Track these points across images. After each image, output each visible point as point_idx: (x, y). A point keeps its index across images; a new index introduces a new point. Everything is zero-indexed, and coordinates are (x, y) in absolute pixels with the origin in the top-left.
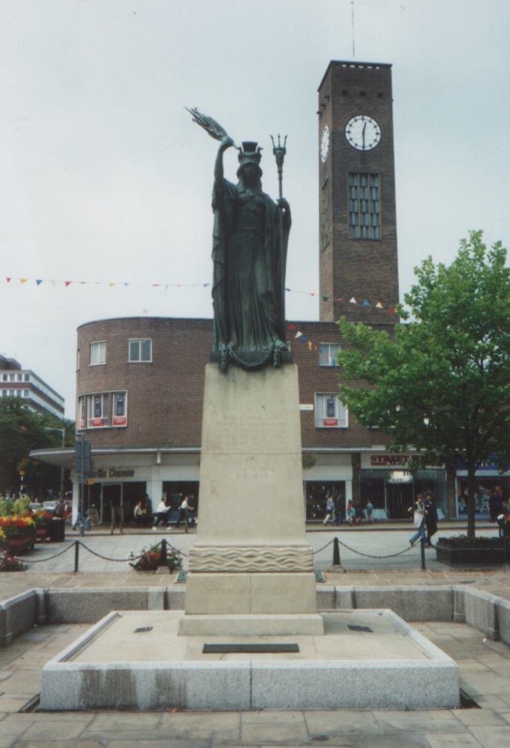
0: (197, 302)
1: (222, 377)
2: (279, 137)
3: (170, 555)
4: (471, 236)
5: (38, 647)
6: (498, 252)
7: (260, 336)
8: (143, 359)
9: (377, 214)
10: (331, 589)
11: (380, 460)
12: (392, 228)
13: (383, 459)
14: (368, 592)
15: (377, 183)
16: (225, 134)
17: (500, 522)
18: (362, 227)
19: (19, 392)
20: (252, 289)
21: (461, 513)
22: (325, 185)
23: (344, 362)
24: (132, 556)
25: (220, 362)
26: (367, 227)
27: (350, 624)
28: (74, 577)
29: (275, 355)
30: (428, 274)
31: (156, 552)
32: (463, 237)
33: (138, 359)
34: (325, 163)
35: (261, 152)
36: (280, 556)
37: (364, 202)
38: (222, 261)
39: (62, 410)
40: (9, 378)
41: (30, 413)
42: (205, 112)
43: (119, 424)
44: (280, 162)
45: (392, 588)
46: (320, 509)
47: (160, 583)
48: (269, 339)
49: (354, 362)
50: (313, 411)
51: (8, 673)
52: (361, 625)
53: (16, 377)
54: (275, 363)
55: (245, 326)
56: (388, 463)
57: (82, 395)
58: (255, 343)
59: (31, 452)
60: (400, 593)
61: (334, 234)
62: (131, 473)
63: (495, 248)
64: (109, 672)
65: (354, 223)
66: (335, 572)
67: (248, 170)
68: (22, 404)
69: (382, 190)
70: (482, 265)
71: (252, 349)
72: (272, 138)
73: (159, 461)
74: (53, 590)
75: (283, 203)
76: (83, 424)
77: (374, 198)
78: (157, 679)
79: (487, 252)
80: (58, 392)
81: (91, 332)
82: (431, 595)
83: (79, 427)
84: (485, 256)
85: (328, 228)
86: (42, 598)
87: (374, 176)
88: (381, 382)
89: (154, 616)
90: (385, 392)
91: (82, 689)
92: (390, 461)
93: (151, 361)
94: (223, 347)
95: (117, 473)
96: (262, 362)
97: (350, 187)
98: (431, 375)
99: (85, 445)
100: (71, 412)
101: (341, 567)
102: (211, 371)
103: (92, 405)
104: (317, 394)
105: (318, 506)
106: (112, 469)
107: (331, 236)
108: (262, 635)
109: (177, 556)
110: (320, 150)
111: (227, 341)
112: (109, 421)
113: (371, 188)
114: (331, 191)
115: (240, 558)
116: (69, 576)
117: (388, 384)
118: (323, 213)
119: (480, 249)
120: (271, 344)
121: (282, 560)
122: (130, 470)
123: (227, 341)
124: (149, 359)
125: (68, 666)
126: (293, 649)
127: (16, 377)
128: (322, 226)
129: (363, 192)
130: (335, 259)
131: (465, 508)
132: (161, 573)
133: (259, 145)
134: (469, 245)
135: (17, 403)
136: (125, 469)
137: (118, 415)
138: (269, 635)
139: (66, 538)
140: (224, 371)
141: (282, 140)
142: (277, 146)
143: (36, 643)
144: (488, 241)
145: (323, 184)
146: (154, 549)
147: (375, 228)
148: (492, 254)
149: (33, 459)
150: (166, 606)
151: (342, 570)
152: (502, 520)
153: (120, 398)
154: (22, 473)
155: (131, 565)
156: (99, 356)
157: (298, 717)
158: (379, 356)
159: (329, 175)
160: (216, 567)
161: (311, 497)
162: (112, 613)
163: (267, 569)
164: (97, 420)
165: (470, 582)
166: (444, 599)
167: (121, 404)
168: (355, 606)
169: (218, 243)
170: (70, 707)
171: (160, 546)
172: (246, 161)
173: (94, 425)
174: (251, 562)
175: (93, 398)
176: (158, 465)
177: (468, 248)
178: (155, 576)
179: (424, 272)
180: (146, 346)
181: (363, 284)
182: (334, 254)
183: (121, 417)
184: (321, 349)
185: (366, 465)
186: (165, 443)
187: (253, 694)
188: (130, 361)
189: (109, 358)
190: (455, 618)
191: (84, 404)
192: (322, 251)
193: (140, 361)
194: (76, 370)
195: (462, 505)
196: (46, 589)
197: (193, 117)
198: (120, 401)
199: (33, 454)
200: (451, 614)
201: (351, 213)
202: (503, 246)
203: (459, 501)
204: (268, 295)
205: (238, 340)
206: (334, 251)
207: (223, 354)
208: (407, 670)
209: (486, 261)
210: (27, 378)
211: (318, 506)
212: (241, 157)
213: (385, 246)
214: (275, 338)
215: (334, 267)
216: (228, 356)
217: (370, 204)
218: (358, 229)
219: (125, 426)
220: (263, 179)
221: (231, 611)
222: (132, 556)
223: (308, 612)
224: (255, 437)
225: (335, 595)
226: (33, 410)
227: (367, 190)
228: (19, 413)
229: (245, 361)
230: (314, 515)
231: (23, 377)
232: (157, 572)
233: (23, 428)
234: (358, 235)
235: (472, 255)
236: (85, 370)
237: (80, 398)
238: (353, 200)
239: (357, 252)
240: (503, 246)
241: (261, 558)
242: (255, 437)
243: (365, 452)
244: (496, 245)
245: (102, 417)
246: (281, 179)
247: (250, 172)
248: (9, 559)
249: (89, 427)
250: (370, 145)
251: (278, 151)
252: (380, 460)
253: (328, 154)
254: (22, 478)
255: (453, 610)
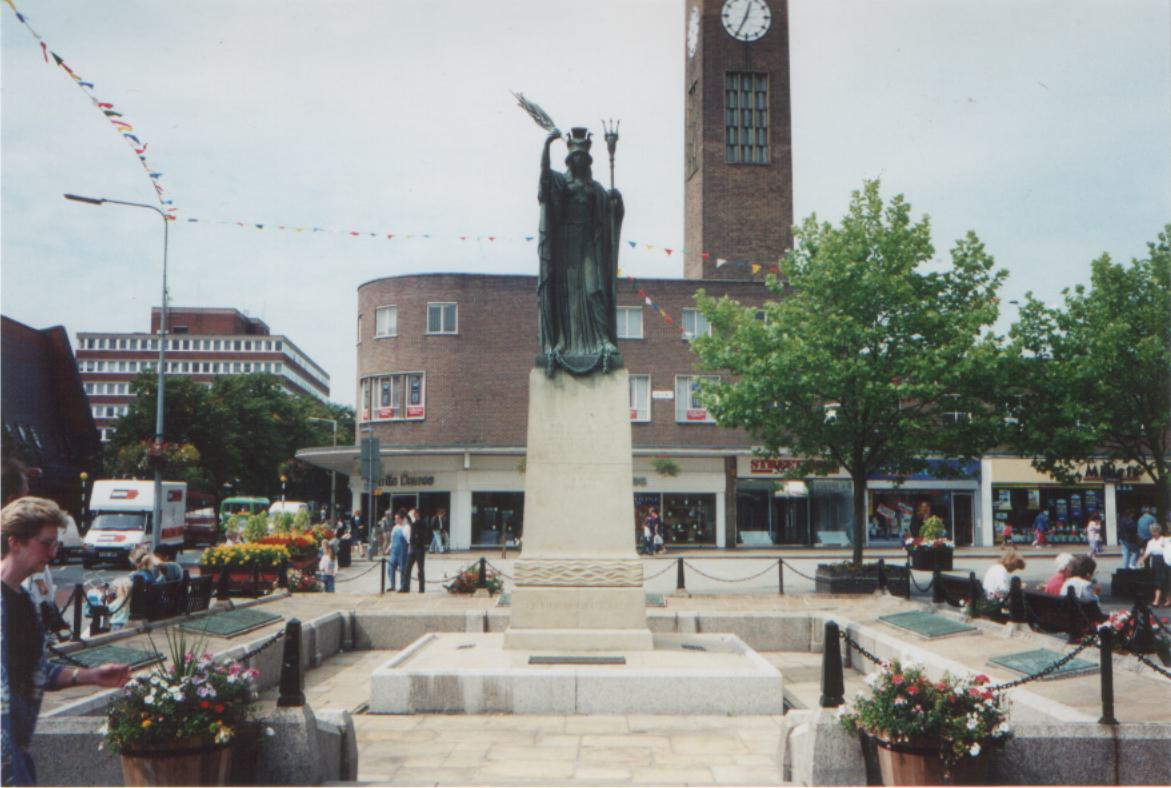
0: (523, 258)
1: (549, 383)
2: (611, 121)
3: (490, 576)
4: (866, 186)
5: (350, 669)
6: (899, 208)
7: (589, 338)
8: (445, 330)
9: (765, 130)
10: (673, 614)
11: (763, 465)
12: (786, 148)
13: (766, 465)
14: (714, 618)
15: (766, 86)
16: (552, 124)
17: (908, 547)
18: (743, 147)
19: (268, 366)
20: (580, 285)
21: (872, 537)
22: (693, 88)
23: (700, 348)
24: (446, 577)
25: (546, 367)
26: (751, 147)
27: (684, 643)
28: (380, 599)
29: (605, 359)
30: (810, 235)
31: (473, 572)
32: (856, 189)
33: (439, 329)
34: (694, 58)
35: (592, 138)
36: (608, 570)
37: (746, 113)
38: (549, 258)
39: (326, 390)
40: (253, 346)
41: (285, 396)
42: (531, 99)
43: (415, 415)
44: (612, 149)
45: (742, 614)
46: (682, 531)
47: (478, 605)
48: (599, 342)
49: (713, 349)
50: (673, 400)
51: (327, 688)
52: (695, 644)
53: (263, 344)
54: (605, 368)
55: (574, 328)
56: (774, 470)
57: (365, 376)
58: (584, 347)
59: (298, 451)
60: (750, 619)
61: (704, 157)
62: (430, 481)
63: (895, 204)
64: (436, 678)
65: (732, 141)
66: (678, 597)
67: (577, 159)
68: (272, 384)
69: (772, 97)
70: (879, 224)
71: (580, 353)
72: (604, 122)
73: (467, 464)
74: (359, 613)
75: (615, 196)
76: (366, 415)
77: (761, 106)
78: (484, 685)
79: (885, 208)
80: (302, 349)
81: (377, 292)
82: (786, 622)
83: (360, 420)
84: (882, 213)
85: (697, 149)
86: (347, 620)
87: (761, 76)
88: (748, 373)
89: (475, 636)
90: (750, 386)
91: (411, 693)
92: (777, 467)
93: (456, 332)
94: (549, 350)
95: (410, 481)
96: (590, 367)
97: (728, 92)
98: (807, 367)
99: (371, 445)
100: (344, 392)
101: (686, 592)
102: (537, 377)
103: (378, 389)
104: (679, 378)
105: (679, 526)
106: (405, 476)
107: (700, 160)
108: (590, 650)
109: (497, 578)
110: (687, 40)
111: (554, 344)
112: (403, 411)
113: (757, 93)
114: (701, 97)
115: (566, 572)
116: (375, 598)
117: (755, 376)
118: (690, 127)
119: (876, 205)
120: (600, 348)
121: (611, 574)
122: (429, 476)
123: (554, 344)
124: (453, 329)
125: (397, 672)
126: (621, 661)
127: (263, 344)
128: (689, 145)
129: (750, 99)
130: (707, 190)
131: (878, 532)
132: (480, 596)
133: (589, 131)
134: (863, 199)
135: (266, 382)
136: (422, 475)
137: (413, 403)
138: (598, 650)
139: (353, 563)
140: (551, 376)
141: (615, 124)
142: (609, 131)
143: (346, 665)
144: (886, 195)
145: (690, 86)
146: (472, 568)
147: (761, 147)
148: (891, 211)
149: (299, 460)
150: (486, 628)
151: (687, 595)
152: (912, 545)
153: (416, 382)
154: (283, 478)
155: (445, 587)
156: (388, 323)
157: (622, 719)
158: (185, 734)
159: (699, 74)
160: (541, 581)
161: (670, 514)
162: (428, 635)
163: (595, 583)
164: (386, 410)
165: (832, 609)
166: (800, 626)
167: (416, 390)
168: (699, 629)
169: (544, 237)
170: (399, 711)
171: (478, 567)
172: (576, 149)
173: (381, 416)
174: (577, 576)
175: (379, 381)
176: (467, 469)
177: (862, 202)
178: (473, 599)
179: (805, 233)
180: (449, 312)
181: (743, 225)
182: (704, 184)
183: (417, 406)
184: (683, 315)
185: (744, 471)
186: (474, 442)
187: (579, 700)
188: (428, 332)
189: (401, 328)
190: (812, 648)
191: (368, 389)
192: (689, 179)
193: (442, 332)
194: (356, 343)
195: (874, 526)
196: (352, 611)
197: (518, 102)
198: (416, 385)
199: (301, 454)
200: (807, 644)
201: (728, 128)
202: (906, 200)
203: (871, 521)
204: (598, 294)
205: (566, 344)
206: (704, 178)
207: (549, 359)
208: (731, 679)
209: (883, 220)
210: (279, 346)
211: (679, 526)
212: (570, 144)
213: (775, 172)
214: (605, 341)
215: (704, 203)
216: (555, 361)
217: (755, 115)
218: (737, 150)
219: (422, 418)
220: (594, 167)
221: (558, 625)
222: (446, 577)
223: (635, 627)
224: (583, 445)
225: (676, 621)
226: (289, 393)
227: (752, 96)
228: (271, 396)
229: (573, 366)
230: (674, 538)
231: (274, 345)
232: (475, 595)
233: (276, 417)
234: (737, 155)
235: (865, 212)
236: (368, 340)
237: (363, 381)
238: (732, 110)
239: (736, 181)
240: (906, 200)
241: (588, 572)
242: (583, 445)
243: (743, 455)
244: (896, 199)
245: (391, 407)
246: (612, 167)
247: (580, 161)
248: (306, 579)
249: (375, 419)
250: (756, 34)
251: (609, 138)
252: (763, 465)
253: (697, 46)
254: (284, 486)
255: (810, 640)
